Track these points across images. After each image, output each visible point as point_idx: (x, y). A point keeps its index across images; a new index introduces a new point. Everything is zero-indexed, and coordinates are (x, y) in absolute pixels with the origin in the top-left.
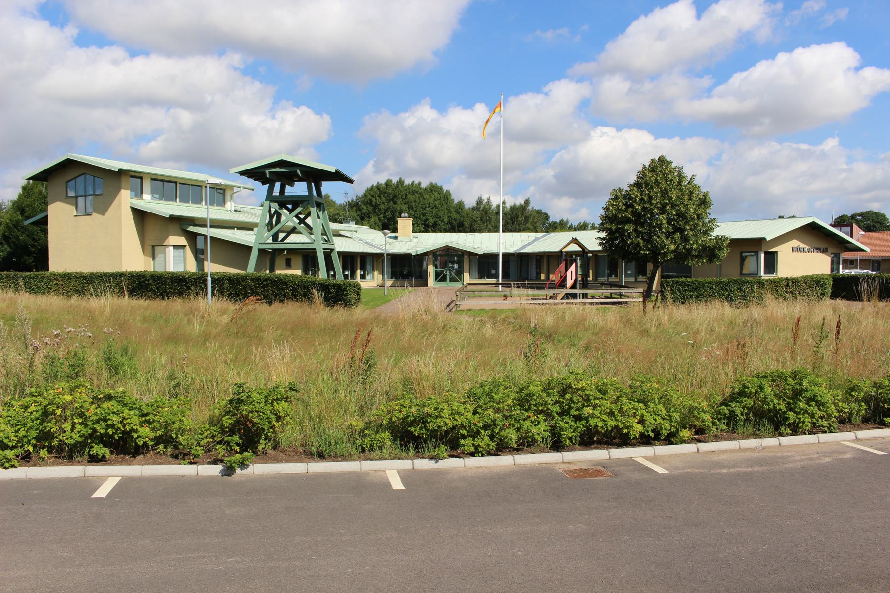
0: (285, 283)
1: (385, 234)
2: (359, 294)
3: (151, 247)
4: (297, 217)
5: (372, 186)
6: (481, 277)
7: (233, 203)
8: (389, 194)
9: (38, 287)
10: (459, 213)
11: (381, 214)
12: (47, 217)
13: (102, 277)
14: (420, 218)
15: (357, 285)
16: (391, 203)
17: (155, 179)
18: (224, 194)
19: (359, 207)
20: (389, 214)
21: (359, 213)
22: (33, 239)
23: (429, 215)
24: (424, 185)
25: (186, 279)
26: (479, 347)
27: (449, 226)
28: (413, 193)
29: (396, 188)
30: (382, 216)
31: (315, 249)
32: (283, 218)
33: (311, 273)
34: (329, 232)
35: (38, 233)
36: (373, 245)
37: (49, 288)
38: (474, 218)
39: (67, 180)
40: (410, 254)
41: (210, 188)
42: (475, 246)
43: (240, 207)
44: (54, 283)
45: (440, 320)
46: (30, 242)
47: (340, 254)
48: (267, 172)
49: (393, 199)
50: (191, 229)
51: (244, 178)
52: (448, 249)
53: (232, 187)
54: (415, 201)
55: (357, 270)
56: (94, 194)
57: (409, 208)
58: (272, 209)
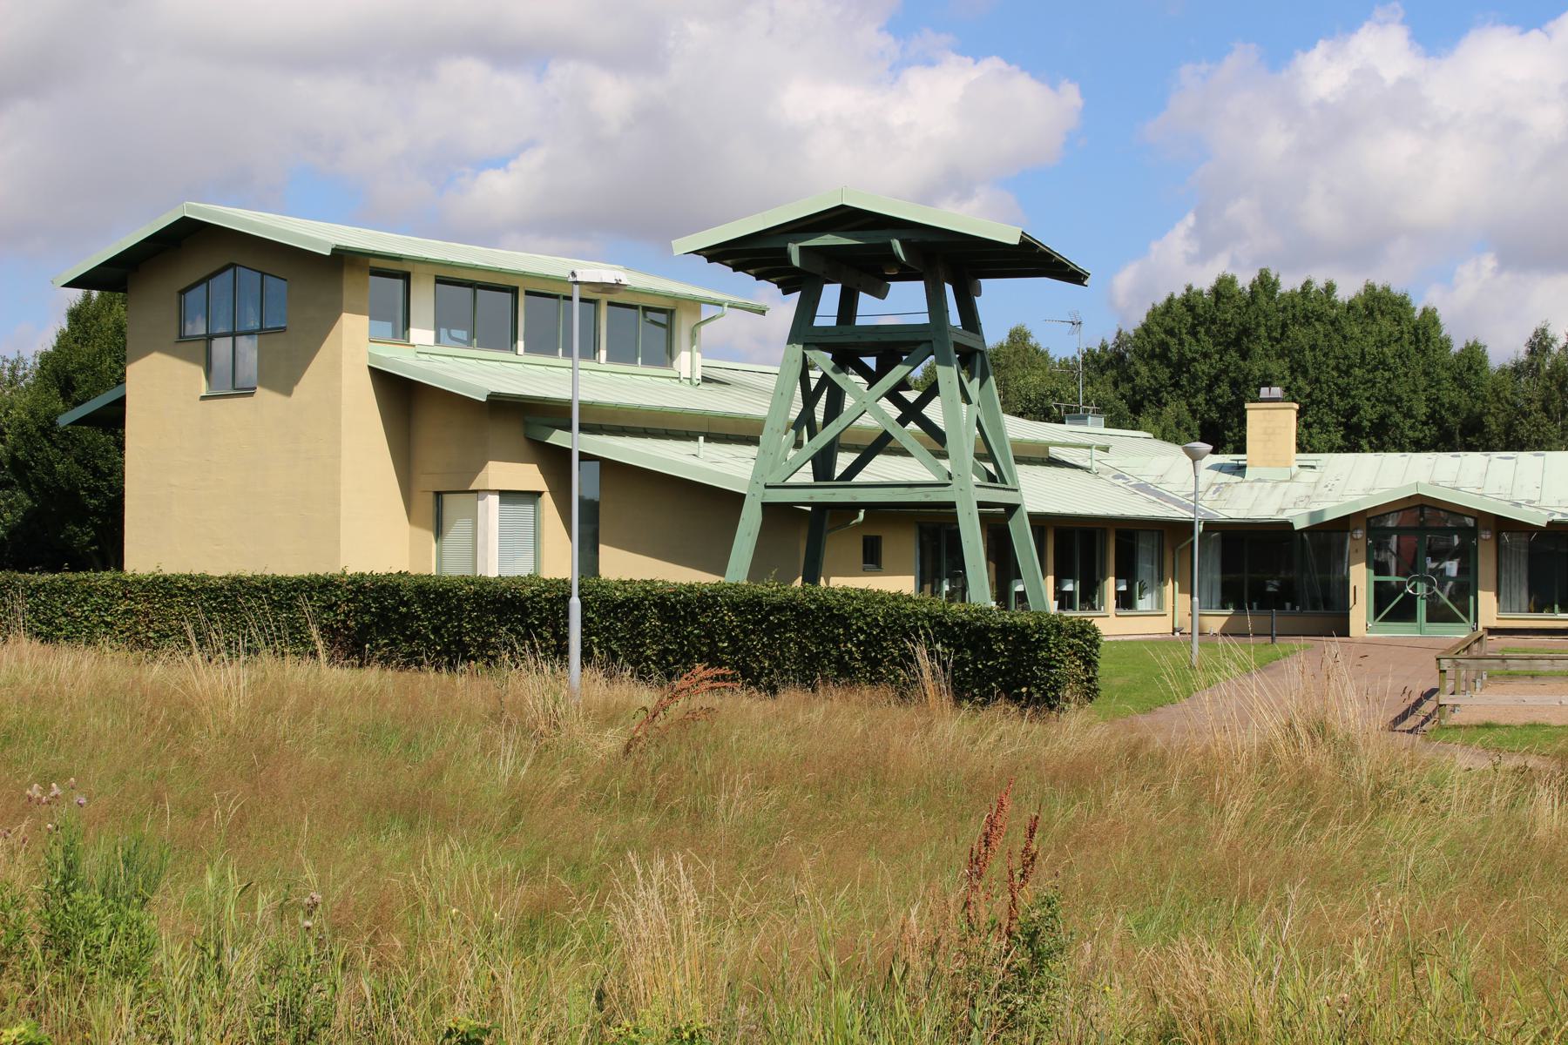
0: (843, 620)
1: (1195, 457)
2: (1090, 663)
3: (431, 497)
4: (893, 395)
5: (1170, 300)
6: (1539, 606)
7: (698, 356)
8: (1225, 324)
9: (74, 620)
10: (1467, 387)
11: (1198, 391)
12: (121, 403)
13: (266, 591)
14: (1330, 405)
15: (1083, 631)
16: (1233, 356)
17: (449, 278)
18: (669, 327)
19: (1125, 371)
20: (1223, 389)
21: (1125, 388)
22: (96, 472)
23: (1360, 393)
24: (1348, 289)
25: (522, 602)
26: (1503, 882)
27: (1431, 431)
28: (1307, 319)
29: (1248, 305)
30: (1201, 398)
31: (952, 505)
32: (849, 402)
33: (946, 588)
34: (1002, 448)
35: (107, 451)
36: (1160, 495)
37: (107, 624)
38: (1521, 402)
39: (182, 287)
40: (1287, 525)
41: (582, 300)
42: (1520, 497)
43: (721, 367)
44: (122, 608)
45: (1363, 768)
46: (86, 478)
47: (1041, 523)
48: (794, 250)
49: (1240, 341)
50: (558, 438)
51: (722, 271)
52: (1422, 507)
53: (695, 304)
54: (1313, 348)
55: (1105, 578)
56: (261, 329)
57: (1293, 371)
58: (812, 373)
